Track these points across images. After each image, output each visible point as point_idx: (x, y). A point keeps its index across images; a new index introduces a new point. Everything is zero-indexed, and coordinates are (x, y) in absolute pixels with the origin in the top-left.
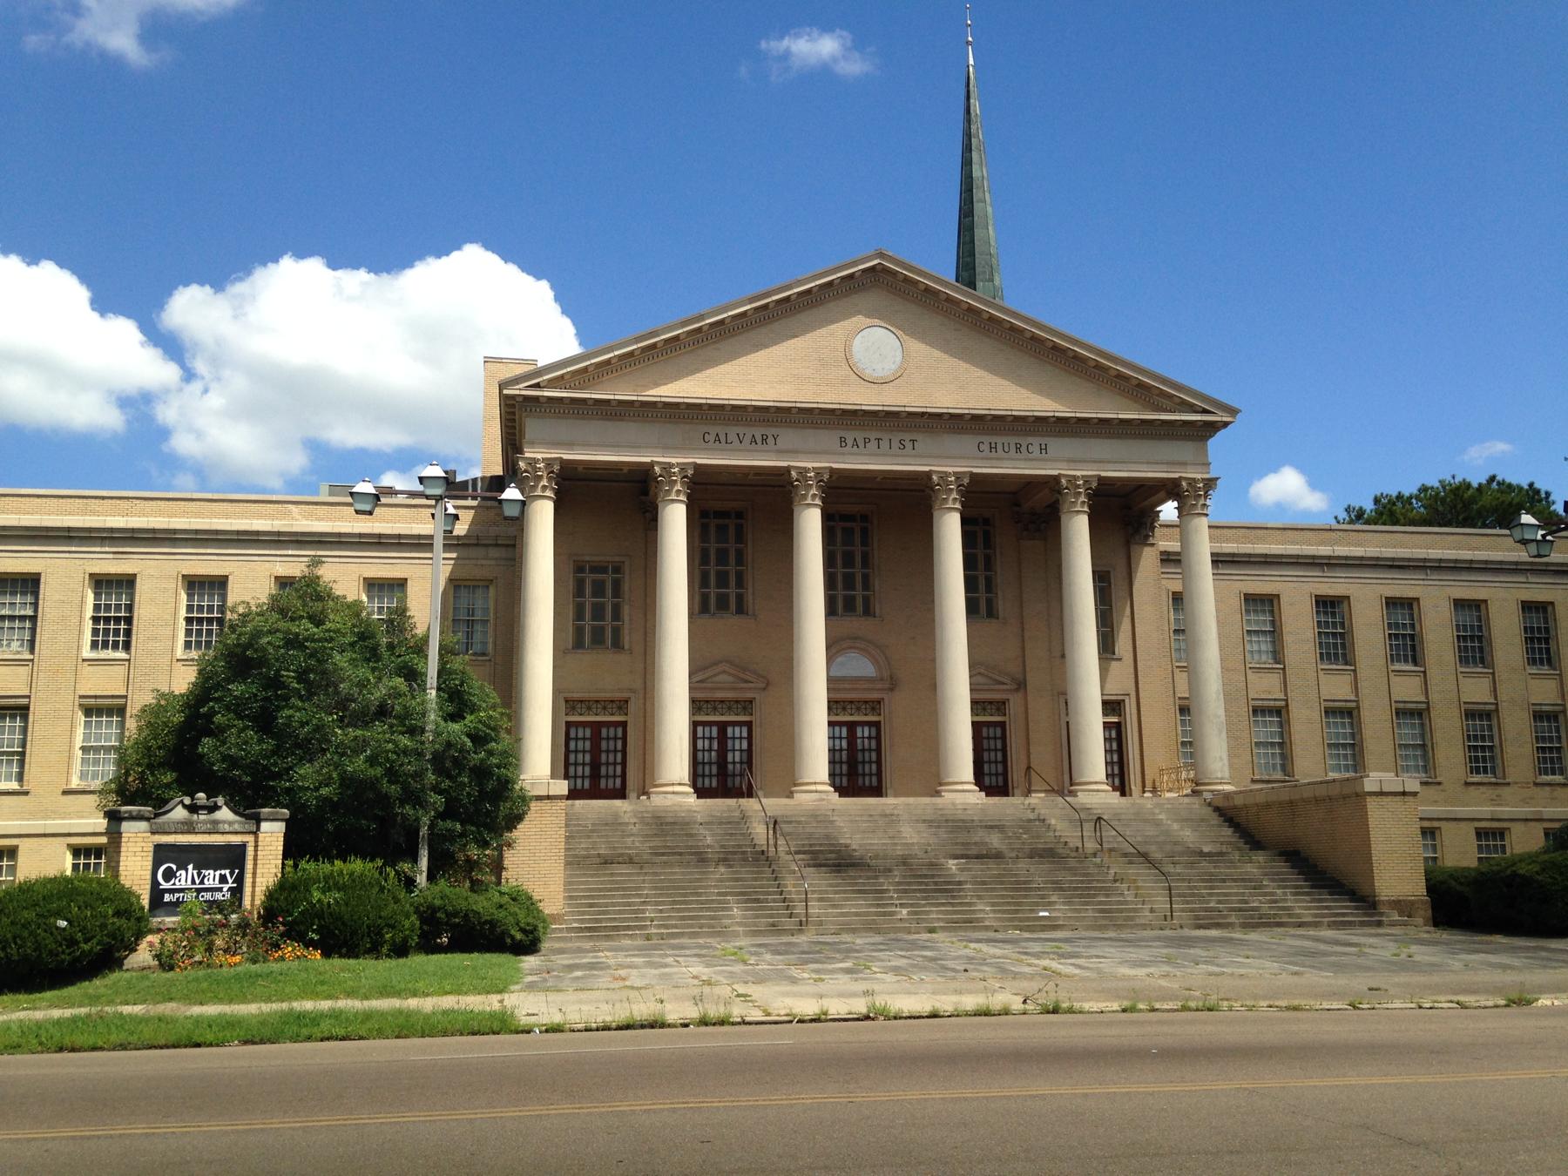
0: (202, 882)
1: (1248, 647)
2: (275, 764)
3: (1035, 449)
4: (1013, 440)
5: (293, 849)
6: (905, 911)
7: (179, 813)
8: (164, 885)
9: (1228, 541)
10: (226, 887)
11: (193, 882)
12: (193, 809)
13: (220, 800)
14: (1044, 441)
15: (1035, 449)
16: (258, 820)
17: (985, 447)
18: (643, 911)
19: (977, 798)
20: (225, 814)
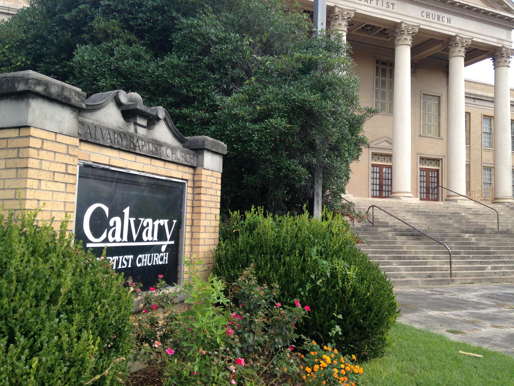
0: (140, 239)
1: (483, 140)
2: (187, 86)
3: (445, 20)
4: (437, 13)
5: (234, 199)
6: (490, 266)
7: (110, 116)
8: (95, 242)
9: (478, 90)
10: (164, 245)
11: (130, 238)
12: (129, 114)
13: (161, 112)
14: (450, 16)
15: (445, 20)
16: (198, 150)
17: (424, 14)
18: (483, 269)
19: (415, 201)
20: (162, 132)
